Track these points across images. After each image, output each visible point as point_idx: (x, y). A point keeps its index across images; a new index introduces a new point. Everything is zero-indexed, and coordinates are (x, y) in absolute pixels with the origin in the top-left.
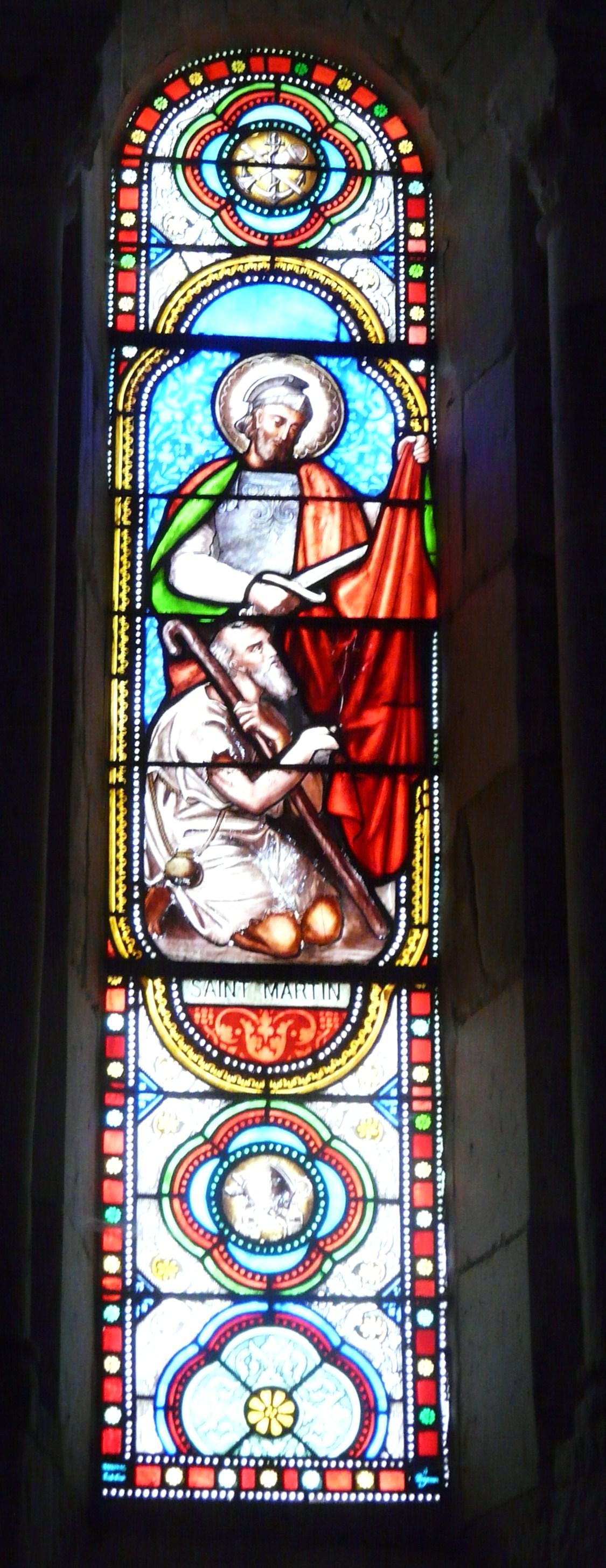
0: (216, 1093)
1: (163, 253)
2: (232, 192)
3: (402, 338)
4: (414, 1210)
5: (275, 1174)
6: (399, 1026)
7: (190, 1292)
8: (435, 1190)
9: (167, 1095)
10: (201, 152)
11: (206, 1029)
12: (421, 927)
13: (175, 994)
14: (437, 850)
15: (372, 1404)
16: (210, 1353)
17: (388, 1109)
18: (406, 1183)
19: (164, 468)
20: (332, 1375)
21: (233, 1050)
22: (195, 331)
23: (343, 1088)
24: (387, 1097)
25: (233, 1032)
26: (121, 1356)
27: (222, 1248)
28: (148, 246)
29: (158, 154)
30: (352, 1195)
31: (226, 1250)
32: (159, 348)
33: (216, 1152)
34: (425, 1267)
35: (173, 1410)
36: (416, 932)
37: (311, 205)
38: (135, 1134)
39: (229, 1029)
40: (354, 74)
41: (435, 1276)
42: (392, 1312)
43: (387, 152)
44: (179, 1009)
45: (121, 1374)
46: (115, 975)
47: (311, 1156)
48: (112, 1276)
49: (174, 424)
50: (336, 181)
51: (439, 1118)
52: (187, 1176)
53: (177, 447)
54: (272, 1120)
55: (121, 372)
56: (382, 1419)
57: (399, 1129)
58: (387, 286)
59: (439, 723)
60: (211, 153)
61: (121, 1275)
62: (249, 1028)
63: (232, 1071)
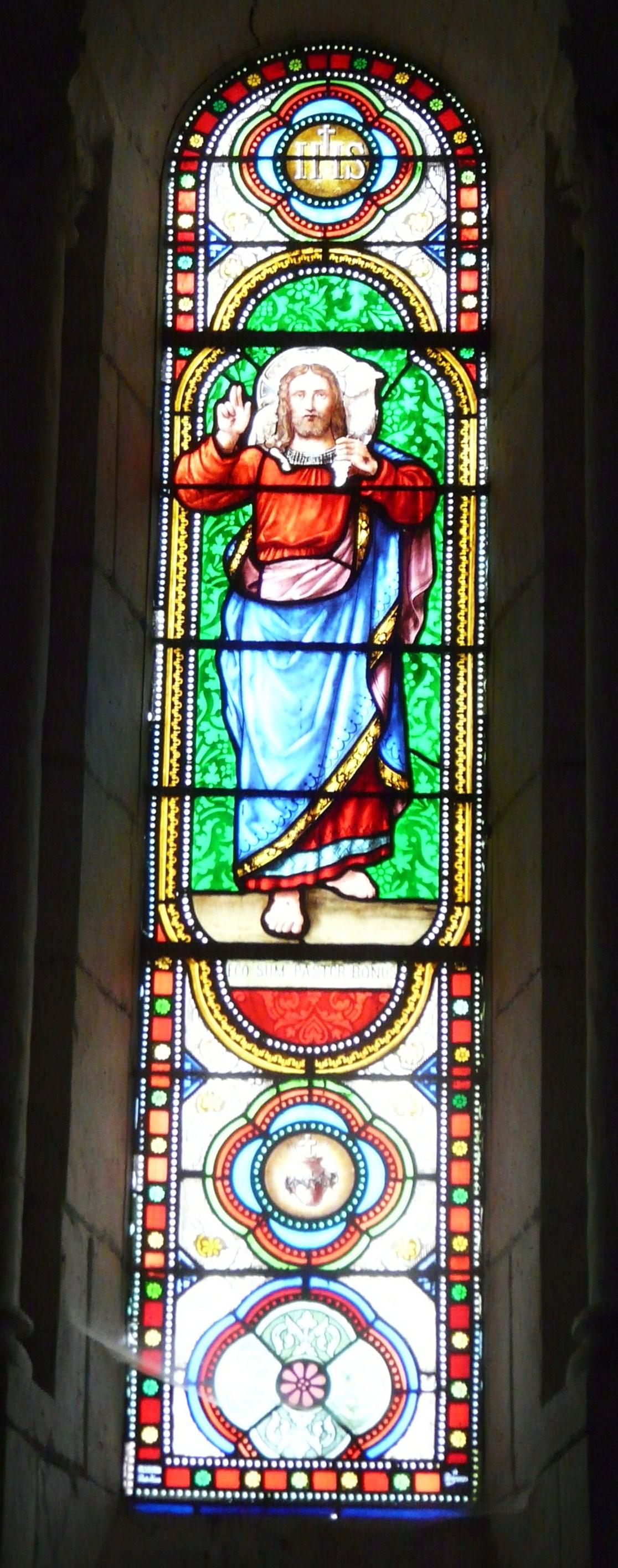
2: (289, 189)
4: (451, 1187)
5: (315, 1163)
6: (440, 1005)
7: (233, 1268)
8: (472, 1313)
9: (236, 245)
10: (257, 149)
12: (462, 905)
14: (480, 713)
18: (444, 1160)
24: (436, 242)
26: (162, 1329)
27: (285, 203)
29: (219, 153)
30: (393, 1175)
31: (289, 204)
32: (216, 349)
34: (460, 1244)
36: (458, 909)
38: (205, 281)
40: (407, 65)
41: (470, 1252)
43: (439, 139)
44: (224, 992)
47: (352, 1135)
48: (160, 1089)
50: (389, 168)
51: (478, 909)
52: (230, 1158)
57: (437, 1106)
59: (488, 383)
60: (268, 148)
61: (171, 1060)
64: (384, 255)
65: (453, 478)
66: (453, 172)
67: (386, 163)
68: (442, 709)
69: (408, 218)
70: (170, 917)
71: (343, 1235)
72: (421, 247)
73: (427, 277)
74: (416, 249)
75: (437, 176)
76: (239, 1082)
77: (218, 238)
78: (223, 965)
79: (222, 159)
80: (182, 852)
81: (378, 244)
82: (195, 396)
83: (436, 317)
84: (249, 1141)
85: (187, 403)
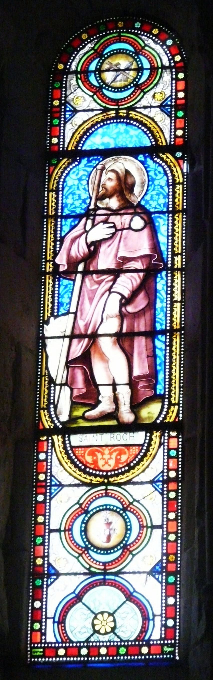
0: (84, 484)
1: (57, 489)
3: (165, 486)
11: (80, 458)
13: (67, 442)
15: (147, 617)
16: (78, 598)
17: (158, 486)
19: (69, 205)
20: (130, 605)
21: (92, 466)
22: (83, 149)
23: (139, 479)
24: (158, 481)
25: (93, 458)
28: (51, 486)
31: (88, 553)
33: (83, 511)
35: (61, 622)
37: (124, 512)
39: (91, 457)
42: (157, 576)
44: (69, 449)
45: (44, 523)
46: (43, 436)
49: (76, 185)
50: (146, 74)
51: (178, 620)
53: (74, 196)
54: (122, 40)
55: (51, 173)
56: (151, 623)
58: (168, 120)
60: (93, 67)
62: (99, 455)
63: (90, 474)
64: (143, 113)
65: (171, 261)
66: (174, 73)
67: (145, 72)
68: (165, 375)
69: (144, 558)
70: (45, 416)
71: (122, 554)
72: (160, 108)
73: (162, 122)
74: (158, 109)
75: (167, 76)
76: (75, 488)
77: (55, 483)
78: (69, 437)
79: (73, 73)
80: (57, 225)
81: (140, 108)
82: (58, 183)
83: (166, 140)
84: (79, 515)
85: (55, 186)
